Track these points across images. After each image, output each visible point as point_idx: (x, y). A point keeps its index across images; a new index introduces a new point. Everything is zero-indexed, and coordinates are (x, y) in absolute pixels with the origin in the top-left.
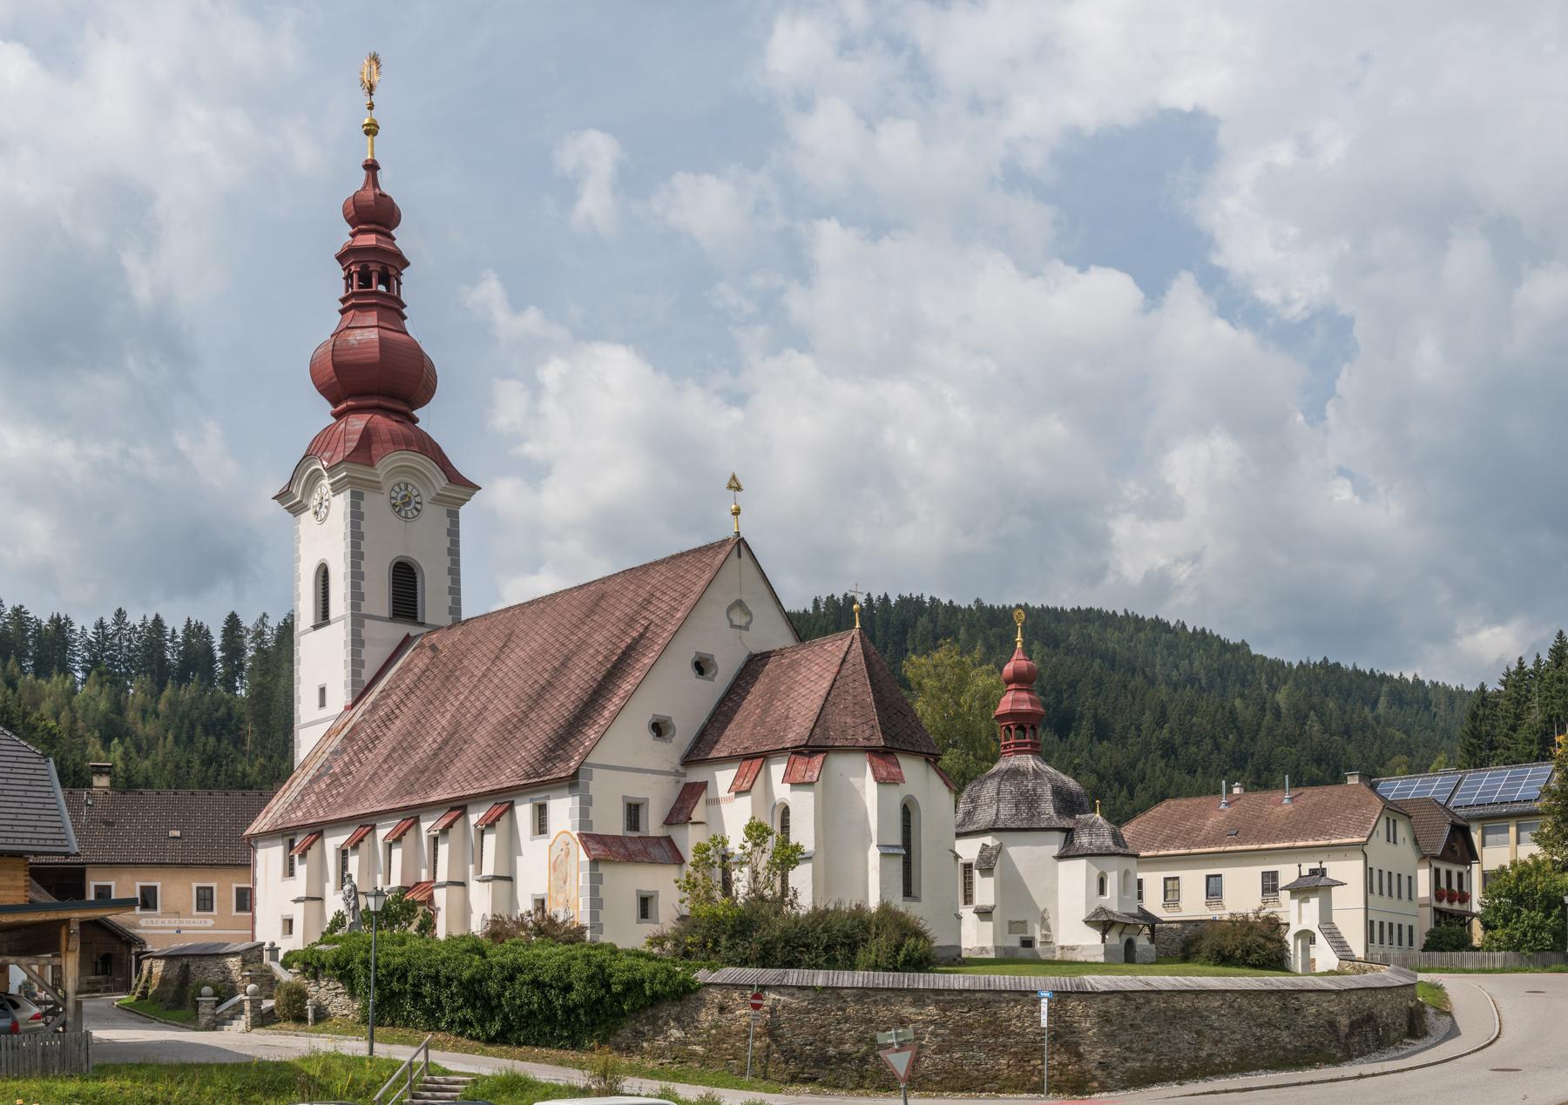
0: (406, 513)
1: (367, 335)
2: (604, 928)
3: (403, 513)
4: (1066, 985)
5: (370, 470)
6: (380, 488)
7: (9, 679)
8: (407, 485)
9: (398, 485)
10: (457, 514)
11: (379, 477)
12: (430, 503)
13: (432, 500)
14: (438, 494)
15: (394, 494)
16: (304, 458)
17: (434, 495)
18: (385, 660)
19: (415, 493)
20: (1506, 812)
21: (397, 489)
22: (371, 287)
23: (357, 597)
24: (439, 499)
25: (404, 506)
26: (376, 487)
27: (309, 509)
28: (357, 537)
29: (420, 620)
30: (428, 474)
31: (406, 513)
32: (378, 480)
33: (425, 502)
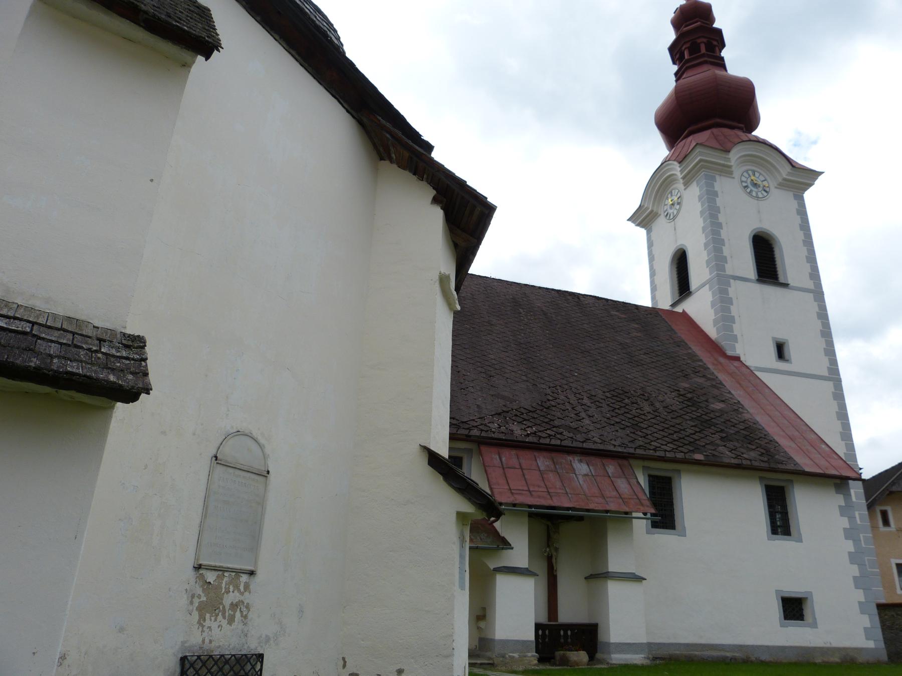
0: (757, 194)
1: (700, 75)
2: (767, 538)
3: (754, 194)
4: (716, 405)
5: (723, 155)
6: (731, 173)
7: (254, 573)
8: (754, 172)
9: (747, 171)
10: (802, 199)
11: (730, 161)
12: (776, 188)
13: (778, 185)
14: (785, 179)
15: (744, 179)
16: (662, 164)
17: (780, 180)
18: (248, 15)
19: (762, 178)
20: (37, 369)
21: (745, 174)
22: (700, 52)
23: (718, 260)
24: (785, 185)
25: (753, 188)
26: (726, 171)
27: (660, 215)
28: (712, 214)
29: (781, 279)
30: (774, 163)
31: (757, 194)
32: (729, 164)
33: (772, 187)
